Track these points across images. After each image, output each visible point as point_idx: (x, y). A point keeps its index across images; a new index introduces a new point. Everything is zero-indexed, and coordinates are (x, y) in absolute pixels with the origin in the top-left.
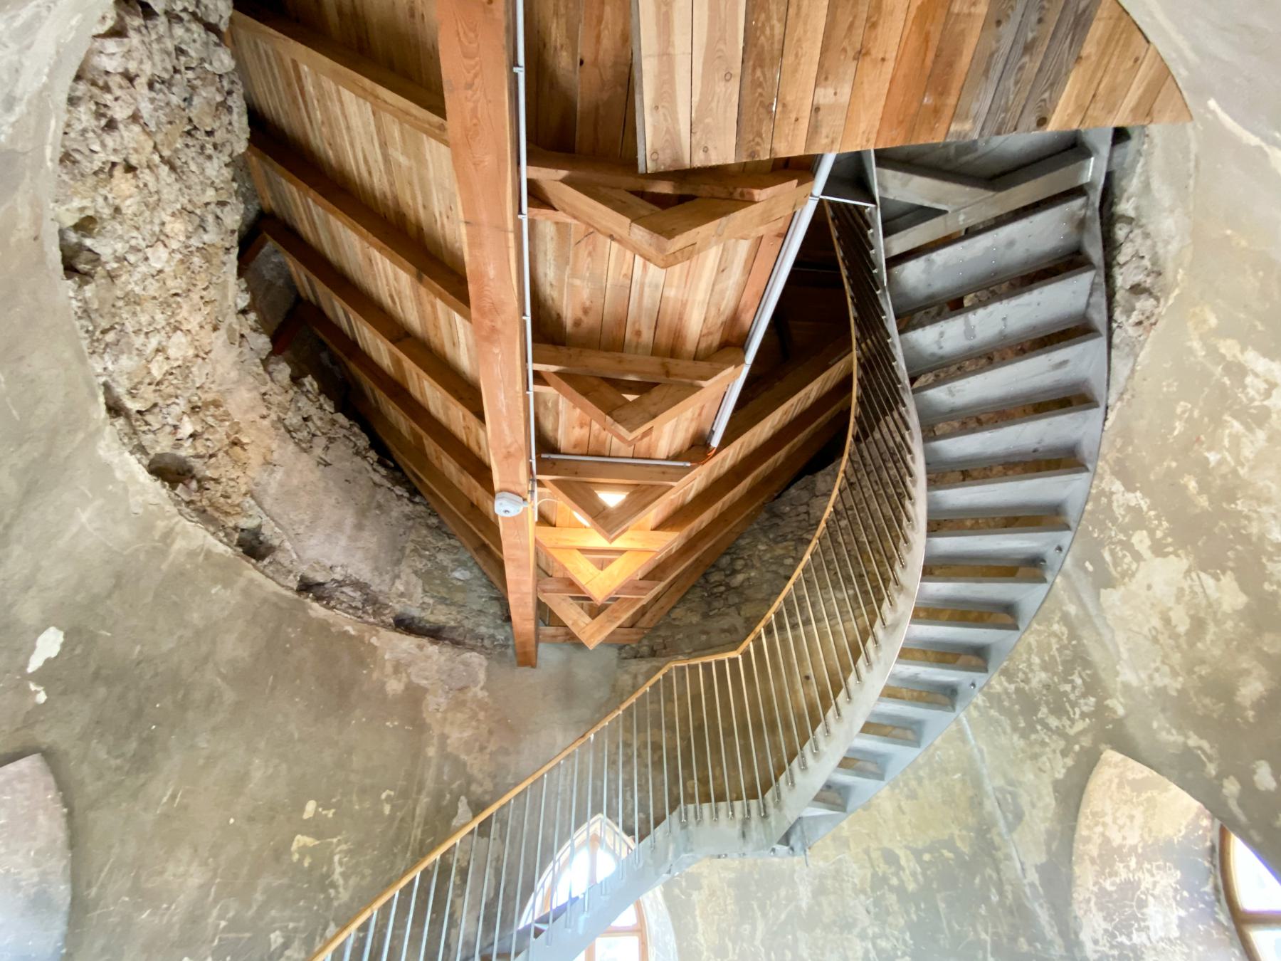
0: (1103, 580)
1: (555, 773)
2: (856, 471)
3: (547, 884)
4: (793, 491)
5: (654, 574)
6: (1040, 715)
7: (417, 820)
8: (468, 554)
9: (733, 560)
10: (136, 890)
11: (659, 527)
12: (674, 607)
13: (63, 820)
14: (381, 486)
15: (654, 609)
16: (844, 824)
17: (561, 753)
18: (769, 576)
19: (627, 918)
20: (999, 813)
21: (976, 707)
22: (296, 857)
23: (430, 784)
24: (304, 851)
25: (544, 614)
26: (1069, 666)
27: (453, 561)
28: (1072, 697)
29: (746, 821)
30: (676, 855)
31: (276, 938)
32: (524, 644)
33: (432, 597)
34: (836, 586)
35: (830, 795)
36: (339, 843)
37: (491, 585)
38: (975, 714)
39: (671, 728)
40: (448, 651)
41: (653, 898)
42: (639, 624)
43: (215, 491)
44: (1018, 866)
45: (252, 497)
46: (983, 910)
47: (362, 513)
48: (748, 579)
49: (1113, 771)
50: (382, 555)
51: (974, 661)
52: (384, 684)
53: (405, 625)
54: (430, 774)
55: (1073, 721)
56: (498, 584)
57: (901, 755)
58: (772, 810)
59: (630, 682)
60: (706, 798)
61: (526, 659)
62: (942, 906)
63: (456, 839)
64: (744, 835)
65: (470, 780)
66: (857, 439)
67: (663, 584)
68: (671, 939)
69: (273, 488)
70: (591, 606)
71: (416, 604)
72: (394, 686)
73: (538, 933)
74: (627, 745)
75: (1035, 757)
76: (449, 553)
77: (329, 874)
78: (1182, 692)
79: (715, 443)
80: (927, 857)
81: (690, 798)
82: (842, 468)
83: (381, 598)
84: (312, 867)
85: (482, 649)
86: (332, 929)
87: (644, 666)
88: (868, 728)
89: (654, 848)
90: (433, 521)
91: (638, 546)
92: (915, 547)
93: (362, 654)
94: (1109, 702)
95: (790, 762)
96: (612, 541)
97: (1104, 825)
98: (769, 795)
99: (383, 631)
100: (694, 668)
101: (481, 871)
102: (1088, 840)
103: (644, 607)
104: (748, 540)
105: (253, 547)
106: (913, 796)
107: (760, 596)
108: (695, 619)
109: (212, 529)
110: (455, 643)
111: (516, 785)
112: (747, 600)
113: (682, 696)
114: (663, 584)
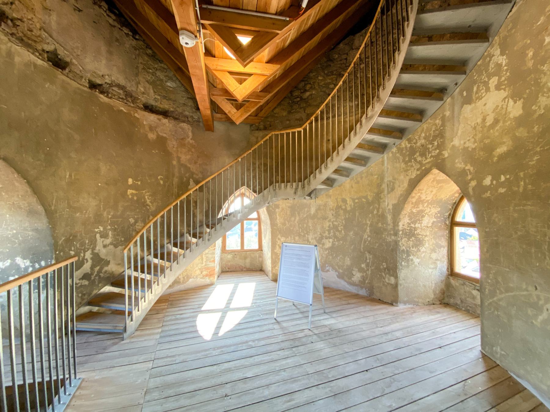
0: (468, 101)
1: (226, 172)
2: (377, 34)
3: (227, 206)
4: (341, 45)
5: (267, 89)
6: (415, 156)
7: (174, 186)
8: (172, 73)
9: (305, 85)
10: (70, 207)
11: (270, 61)
12: (275, 108)
13: (27, 184)
14: (114, 26)
15: (266, 108)
16: (331, 191)
17: (226, 165)
18: (322, 93)
19: (254, 215)
20: (386, 188)
21: (392, 153)
22: (130, 197)
23: (177, 174)
24: (132, 194)
25: (215, 107)
26: (435, 137)
27: (166, 76)
28: (430, 150)
29: (296, 189)
30: (271, 198)
31: (132, 220)
32: (207, 121)
33: (159, 95)
34: (351, 100)
35: (329, 182)
36: (146, 192)
37: (186, 91)
38: (391, 155)
39: (271, 158)
40: (173, 122)
41: (263, 211)
42: (259, 115)
43: (24, 27)
44: (387, 204)
45: (45, 31)
46: (370, 216)
47: (109, 43)
48: (311, 95)
49: (433, 176)
50: (127, 70)
51: (398, 134)
52: (147, 135)
53: (148, 108)
54: (176, 170)
55: (426, 158)
56: (191, 91)
57: (358, 169)
58: (306, 185)
59: (255, 140)
60: (283, 181)
61: (209, 128)
62: (357, 214)
63: (191, 192)
64: (295, 193)
65: (193, 173)
66: (382, 12)
67: (271, 95)
68: (268, 222)
69: (54, 25)
70: (236, 104)
71: (152, 98)
72: (152, 136)
73: (224, 219)
74: (254, 164)
75: (406, 171)
76: (162, 71)
77: (145, 202)
78: (474, 149)
79: (304, 5)
80: (356, 201)
81: (277, 182)
82: (370, 30)
83: (133, 94)
84: (137, 200)
85: (188, 122)
86: (151, 217)
87: (261, 134)
88: (348, 159)
89: (263, 196)
90: (149, 51)
91: (259, 72)
92: (392, 79)
93: (135, 123)
94: (443, 152)
95: (315, 170)
96: (245, 66)
97: (421, 193)
98: (306, 181)
99: (139, 111)
100: (282, 135)
101: (202, 203)
102: (414, 197)
103: (261, 106)
104: (314, 74)
105: (58, 63)
106: (358, 183)
107: (315, 104)
108: (285, 114)
109: (30, 50)
110: (175, 119)
111: (211, 175)
112: (310, 105)
113: (277, 147)
114: (271, 95)
